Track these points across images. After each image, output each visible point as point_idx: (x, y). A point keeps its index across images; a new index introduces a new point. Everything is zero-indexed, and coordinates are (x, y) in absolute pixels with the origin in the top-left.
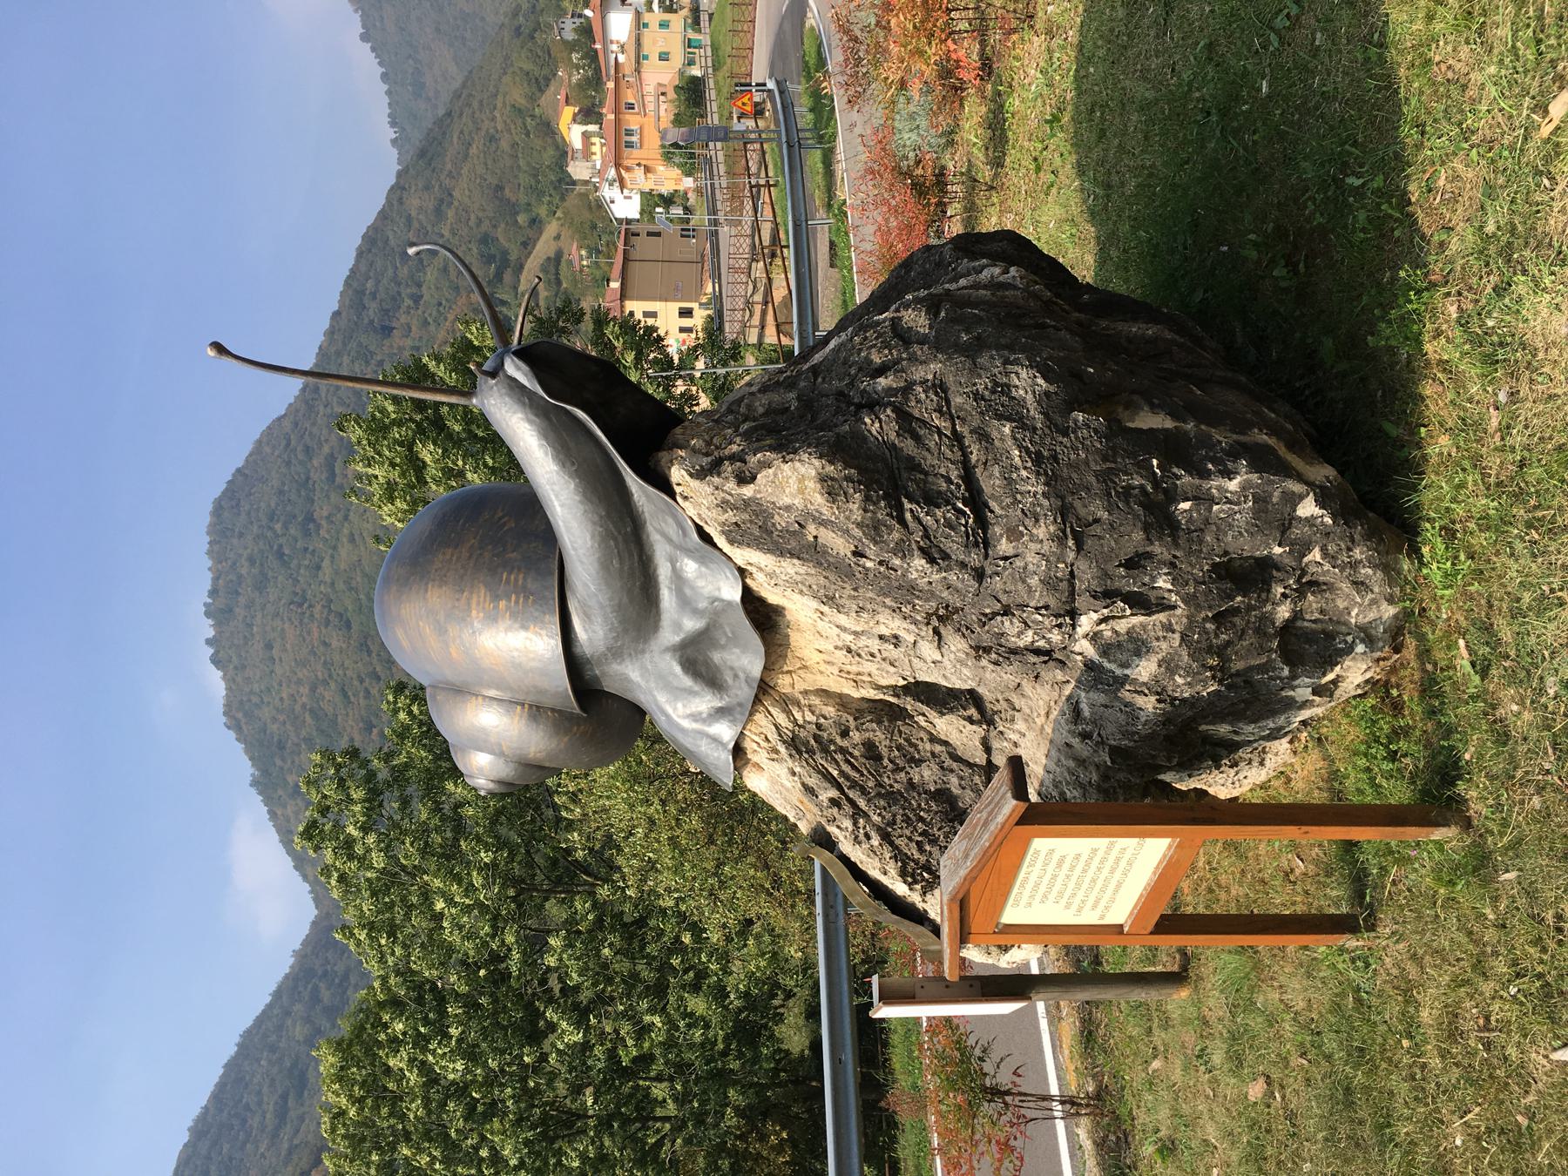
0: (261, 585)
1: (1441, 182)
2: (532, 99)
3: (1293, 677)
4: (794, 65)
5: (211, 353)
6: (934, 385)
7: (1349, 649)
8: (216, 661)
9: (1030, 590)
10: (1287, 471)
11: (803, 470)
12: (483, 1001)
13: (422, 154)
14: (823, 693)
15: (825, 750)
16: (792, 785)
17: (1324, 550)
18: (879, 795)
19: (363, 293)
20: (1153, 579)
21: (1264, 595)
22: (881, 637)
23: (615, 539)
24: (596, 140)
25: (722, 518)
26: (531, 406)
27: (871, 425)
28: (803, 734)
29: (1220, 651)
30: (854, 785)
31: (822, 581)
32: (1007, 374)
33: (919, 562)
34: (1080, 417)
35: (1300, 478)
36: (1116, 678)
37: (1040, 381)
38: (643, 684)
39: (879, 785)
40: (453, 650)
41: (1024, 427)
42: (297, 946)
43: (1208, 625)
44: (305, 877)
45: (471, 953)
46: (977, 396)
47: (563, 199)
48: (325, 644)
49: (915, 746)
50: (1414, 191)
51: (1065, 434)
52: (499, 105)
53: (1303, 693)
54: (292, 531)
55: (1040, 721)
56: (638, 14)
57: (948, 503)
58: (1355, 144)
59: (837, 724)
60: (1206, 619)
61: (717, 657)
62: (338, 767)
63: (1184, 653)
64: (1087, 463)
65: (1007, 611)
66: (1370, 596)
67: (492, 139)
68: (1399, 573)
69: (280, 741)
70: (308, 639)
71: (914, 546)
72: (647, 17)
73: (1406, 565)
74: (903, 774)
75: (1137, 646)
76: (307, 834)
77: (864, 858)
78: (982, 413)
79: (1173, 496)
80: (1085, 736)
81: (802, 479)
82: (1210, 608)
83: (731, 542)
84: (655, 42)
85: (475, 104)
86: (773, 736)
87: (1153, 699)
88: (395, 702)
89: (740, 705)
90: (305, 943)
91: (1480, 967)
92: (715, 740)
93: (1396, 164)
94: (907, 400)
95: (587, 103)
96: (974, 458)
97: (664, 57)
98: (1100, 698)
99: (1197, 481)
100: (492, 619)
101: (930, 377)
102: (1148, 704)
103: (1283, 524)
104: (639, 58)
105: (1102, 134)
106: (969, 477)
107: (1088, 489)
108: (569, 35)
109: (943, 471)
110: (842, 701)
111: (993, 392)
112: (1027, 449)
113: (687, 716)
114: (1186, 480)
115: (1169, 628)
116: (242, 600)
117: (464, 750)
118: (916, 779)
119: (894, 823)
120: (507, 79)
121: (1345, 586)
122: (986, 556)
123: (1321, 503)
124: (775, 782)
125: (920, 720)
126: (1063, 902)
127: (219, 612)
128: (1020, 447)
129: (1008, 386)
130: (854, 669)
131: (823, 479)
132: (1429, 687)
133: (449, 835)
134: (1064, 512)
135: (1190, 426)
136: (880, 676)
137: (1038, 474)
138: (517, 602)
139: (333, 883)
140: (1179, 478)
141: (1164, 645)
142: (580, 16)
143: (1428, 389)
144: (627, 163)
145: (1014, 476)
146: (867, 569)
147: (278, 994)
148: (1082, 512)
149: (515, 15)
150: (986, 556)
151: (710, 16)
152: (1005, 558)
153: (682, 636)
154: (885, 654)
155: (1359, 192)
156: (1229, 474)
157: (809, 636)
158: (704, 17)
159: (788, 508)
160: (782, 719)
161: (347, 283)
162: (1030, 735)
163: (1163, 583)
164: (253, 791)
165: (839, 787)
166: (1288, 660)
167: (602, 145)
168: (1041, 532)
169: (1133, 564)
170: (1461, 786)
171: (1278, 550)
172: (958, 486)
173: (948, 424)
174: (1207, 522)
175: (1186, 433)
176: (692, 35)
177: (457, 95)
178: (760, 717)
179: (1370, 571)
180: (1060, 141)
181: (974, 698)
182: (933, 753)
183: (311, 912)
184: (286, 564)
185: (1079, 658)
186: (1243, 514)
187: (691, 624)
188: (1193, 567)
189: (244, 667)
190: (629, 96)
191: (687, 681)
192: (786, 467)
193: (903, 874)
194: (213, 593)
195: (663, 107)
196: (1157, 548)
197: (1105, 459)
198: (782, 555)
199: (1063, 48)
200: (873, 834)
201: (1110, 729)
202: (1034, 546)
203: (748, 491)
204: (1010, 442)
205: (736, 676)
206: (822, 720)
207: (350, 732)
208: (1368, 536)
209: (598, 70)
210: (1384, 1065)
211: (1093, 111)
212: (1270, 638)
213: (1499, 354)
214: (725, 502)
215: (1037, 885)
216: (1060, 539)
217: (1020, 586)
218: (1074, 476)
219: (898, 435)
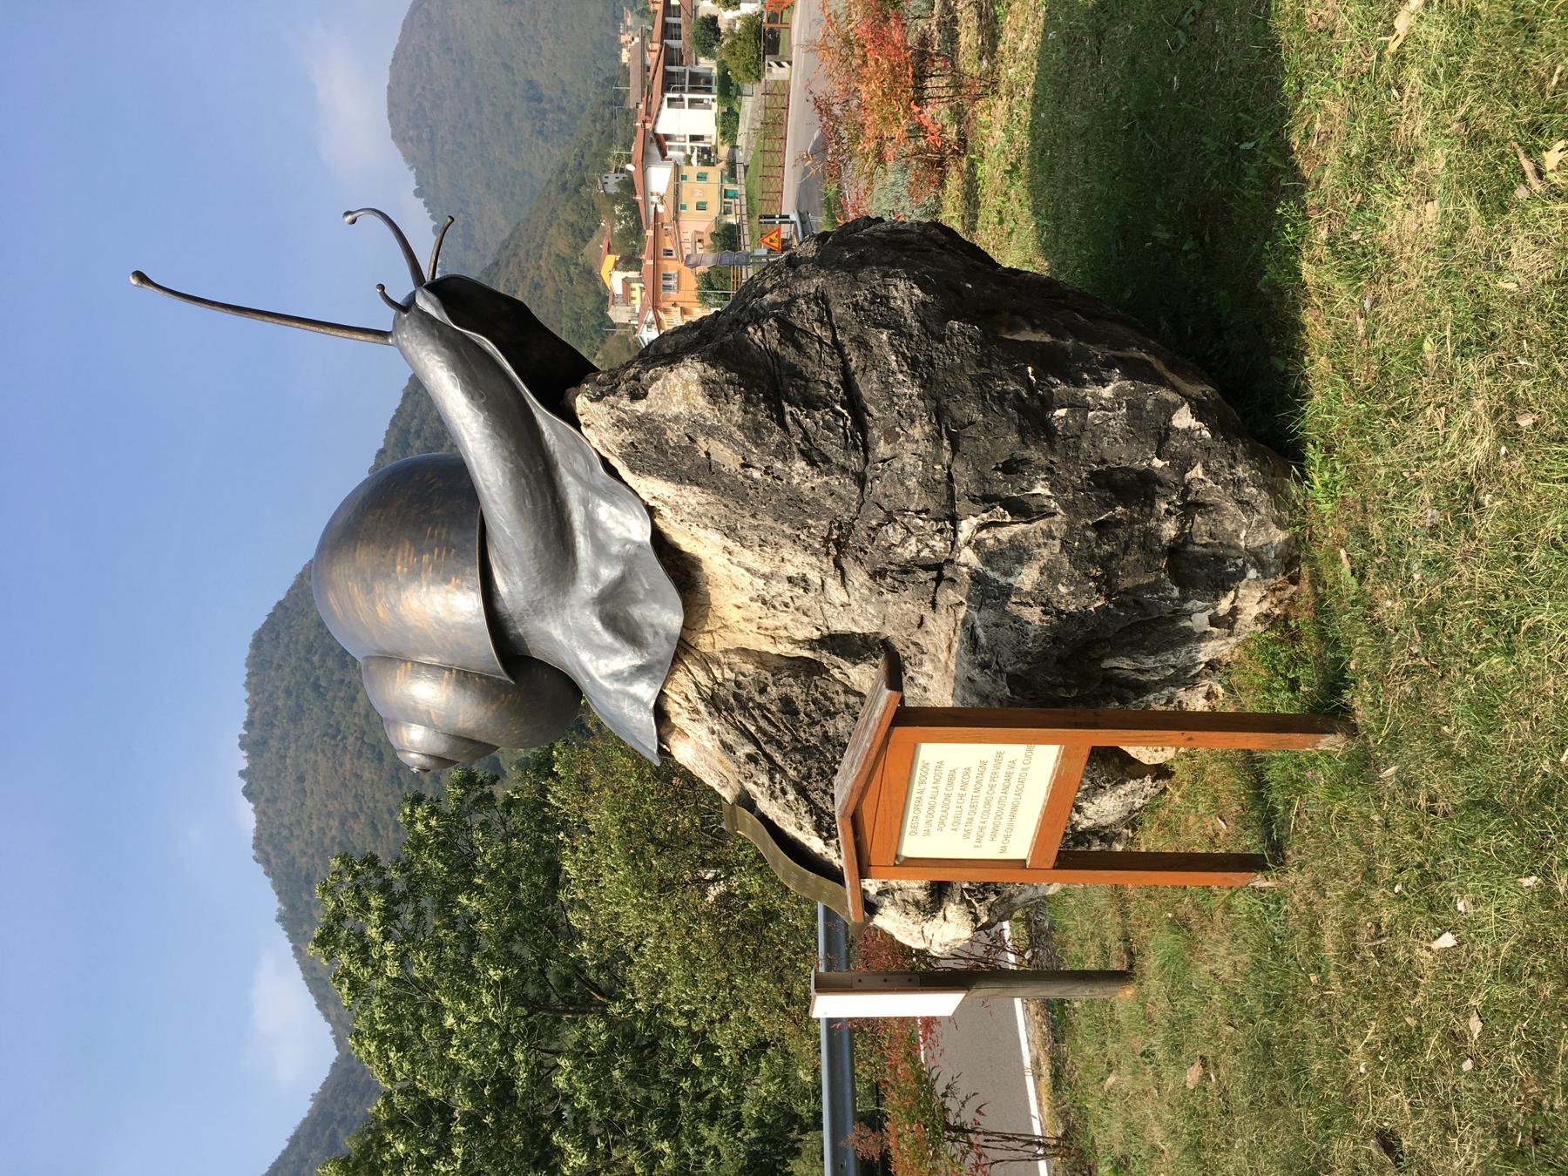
0: (295, 718)
1: (1318, 126)
2: (576, 248)
3: (1185, 599)
4: (818, 200)
5: (134, 281)
6: (816, 298)
7: (1242, 574)
8: (248, 793)
9: (909, 493)
10: (1160, 381)
11: (686, 374)
12: (488, 1120)
14: (744, 652)
15: (744, 707)
16: (711, 744)
17: (1206, 467)
18: (795, 749)
19: (408, 432)
20: (1031, 485)
21: (1147, 510)
22: (790, 579)
23: (526, 477)
24: (636, 286)
25: (619, 439)
26: (440, 338)
27: (754, 335)
28: (722, 692)
29: (1104, 563)
30: (771, 740)
31: (723, 510)
32: (886, 286)
33: (800, 465)
34: (956, 325)
35: (1174, 389)
36: (1000, 587)
37: (917, 291)
38: (565, 642)
39: (795, 739)
40: (380, 610)
41: (901, 334)
42: (317, 1090)
43: (1089, 533)
44: (327, 1017)
45: (478, 1071)
46: (857, 307)
47: (603, 342)
48: (357, 776)
49: (831, 700)
50: (1295, 139)
51: (941, 340)
52: (545, 255)
53: (1200, 621)
54: (329, 663)
55: (943, 657)
56: (677, 167)
57: (826, 406)
58: (1247, 111)
59: (756, 681)
60: (1086, 526)
61: (637, 612)
62: (356, 875)
63: (1065, 560)
64: (962, 368)
65: (890, 518)
66: (1257, 517)
67: (537, 286)
68: (1287, 497)
69: (307, 876)
70: (341, 771)
71: (795, 449)
72: (685, 170)
73: (1294, 490)
74: (818, 728)
75: (1019, 553)
76: (321, 942)
77: (780, 813)
78: (861, 322)
79: (1048, 403)
80: (984, 666)
81: (685, 386)
82: (1090, 515)
83: (632, 469)
84: (692, 192)
85: (522, 254)
86: (693, 695)
87: (1038, 609)
88: (412, 816)
89: (660, 662)
90: (324, 1086)
91: (1369, 874)
92: (636, 700)
93: (1278, 118)
94: (790, 311)
95: (628, 251)
96: (853, 365)
97: (701, 206)
98: (989, 615)
99: (1072, 389)
100: (415, 574)
101: (813, 290)
102: (1033, 615)
103: (1162, 436)
104: (678, 207)
105: (1051, 169)
107: (963, 393)
108: (612, 189)
109: (823, 377)
110: (761, 659)
111: (873, 303)
112: (904, 356)
113: (602, 667)
114: (1061, 388)
115: (1049, 535)
116: (277, 732)
117: (395, 722)
119: (810, 776)
120: (553, 231)
121: (1230, 506)
122: (866, 461)
123: (1198, 413)
124: (698, 748)
125: (835, 672)
126: (961, 828)
127: (254, 745)
128: (896, 353)
129: (887, 298)
130: (769, 623)
131: (704, 382)
132: (1322, 610)
133: (463, 951)
134: (939, 414)
135: (1069, 342)
136: (792, 632)
137: (914, 376)
138: (439, 555)
139: (345, 990)
140: (1054, 386)
141: (1045, 552)
142: (622, 171)
143: (1307, 317)
144: (664, 305)
145: (891, 380)
146: (755, 481)
147: (295, 1140)
148: (957, 414)
149: (562, 172)
150: (866, 461)
151: (746, 168)
152: (884, 461)
153: (600, 587)
154: (798, 603)
155: (1251, 155)
156: (1103, 382)
157: (726, 590)
158: (740, 169)
159: (676, 419)
160: (701, 677)
161: (393, 423)
162: (937, 676)
163: (1041, 489)
164: (279, 927)
165: (756, 743)
166: (1178, 582)
167: (642, 289)
168: (916, 432)
169: (1012, 467)
170: (1347, 694)
171: (1158, 463)
172: (837, 390)
173: (829, 334)
174: (1083, 428)
175: (1064, 349)
176: (728, 186)
178: (680, 676)
179: (1254, 491)
180: (1019, 189)
181: (886, 645)
182: (847, 706)
183: (332, 1053)
184: (321, 696)
185: (965, 570)
186: (1118, 420)
187: (609, 573)
188: (1071, 473)
189: (276, 799)
191: (607, 638)
192: (672, 376)
193: (818, 828)
194: (249, 725)
196: (1034, 454)
197: (980, 364)
198: (681, 482)
199: (1020, 103)
200: (789, 789)
201: (1006, 654)
202: (910, 447)
203: (640, 407)
204: (887, 348)
205: (656, 633)
206: (741, 678)
207: (363, 842)
208: (1250, 454)
209: (638, 221)
210: (1296, 1007)
211: (1044, 151)
212: (1157, 556)
213: (1361, 263)
214: (620, 420)
215: (932, 808)
216: (936, 439)
217: (899, 489)
218: (949, 379)
219: (780, 343)
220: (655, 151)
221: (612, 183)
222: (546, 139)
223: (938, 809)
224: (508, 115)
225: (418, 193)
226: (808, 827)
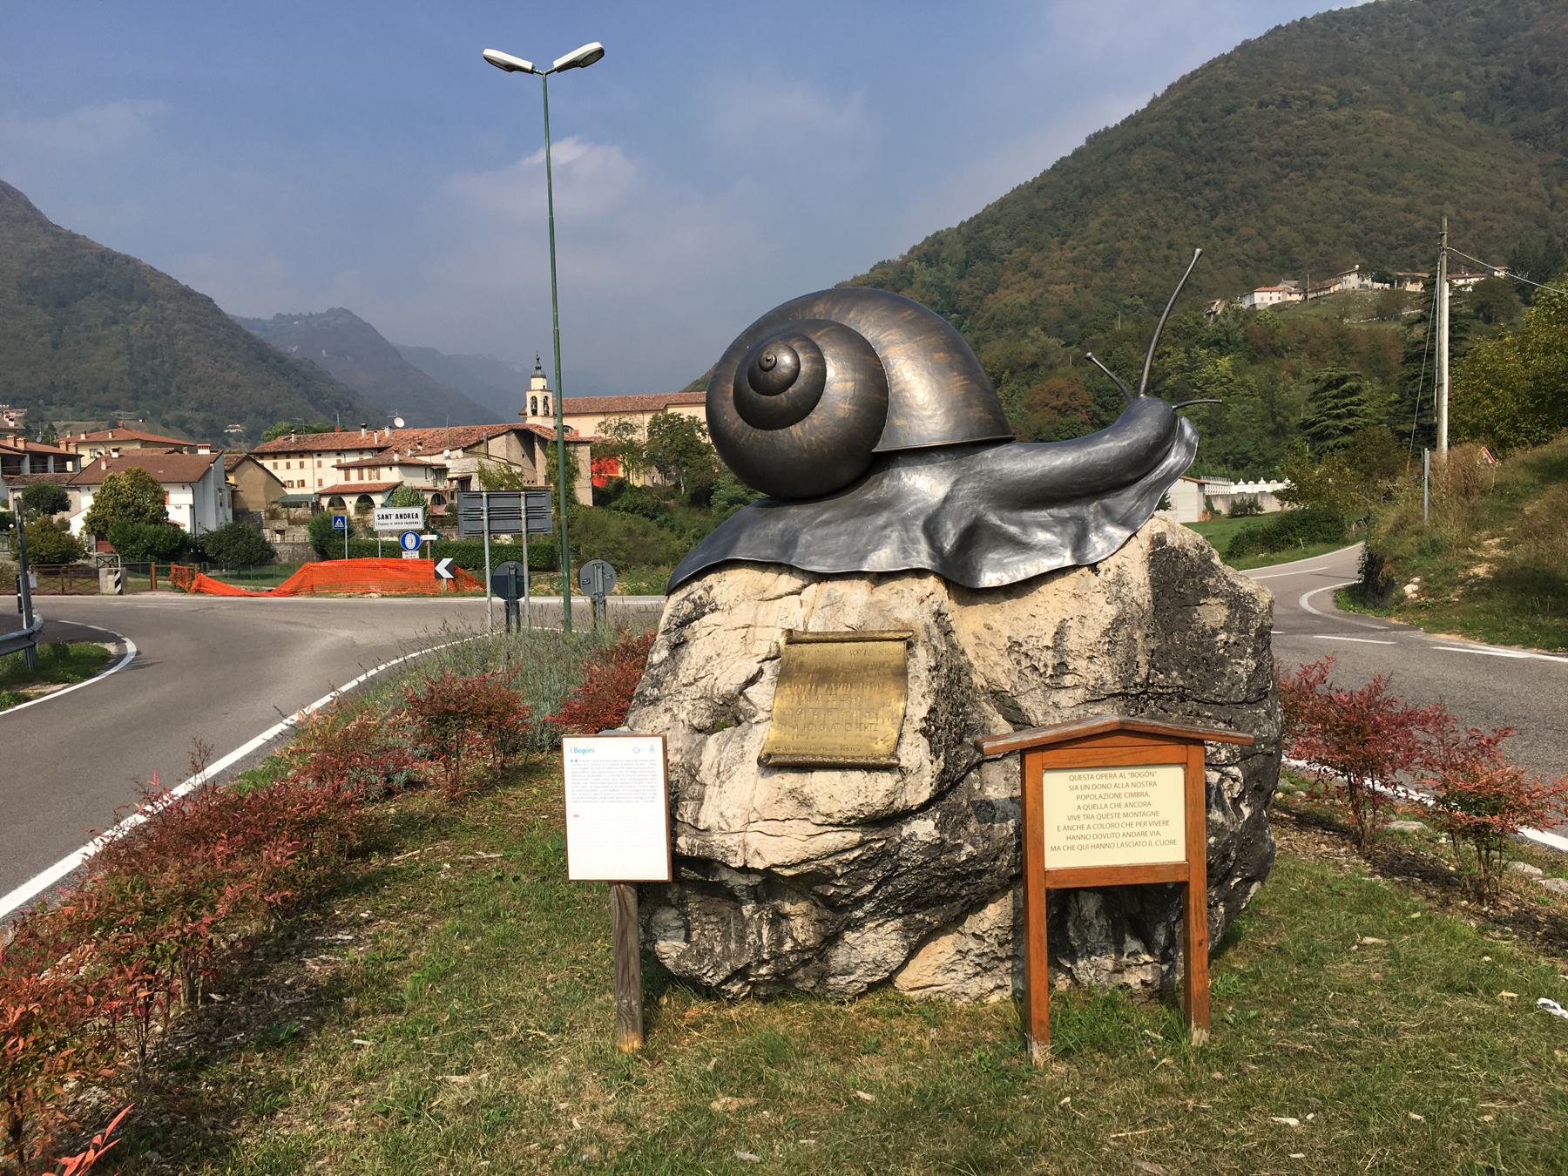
223: (1104, 791)
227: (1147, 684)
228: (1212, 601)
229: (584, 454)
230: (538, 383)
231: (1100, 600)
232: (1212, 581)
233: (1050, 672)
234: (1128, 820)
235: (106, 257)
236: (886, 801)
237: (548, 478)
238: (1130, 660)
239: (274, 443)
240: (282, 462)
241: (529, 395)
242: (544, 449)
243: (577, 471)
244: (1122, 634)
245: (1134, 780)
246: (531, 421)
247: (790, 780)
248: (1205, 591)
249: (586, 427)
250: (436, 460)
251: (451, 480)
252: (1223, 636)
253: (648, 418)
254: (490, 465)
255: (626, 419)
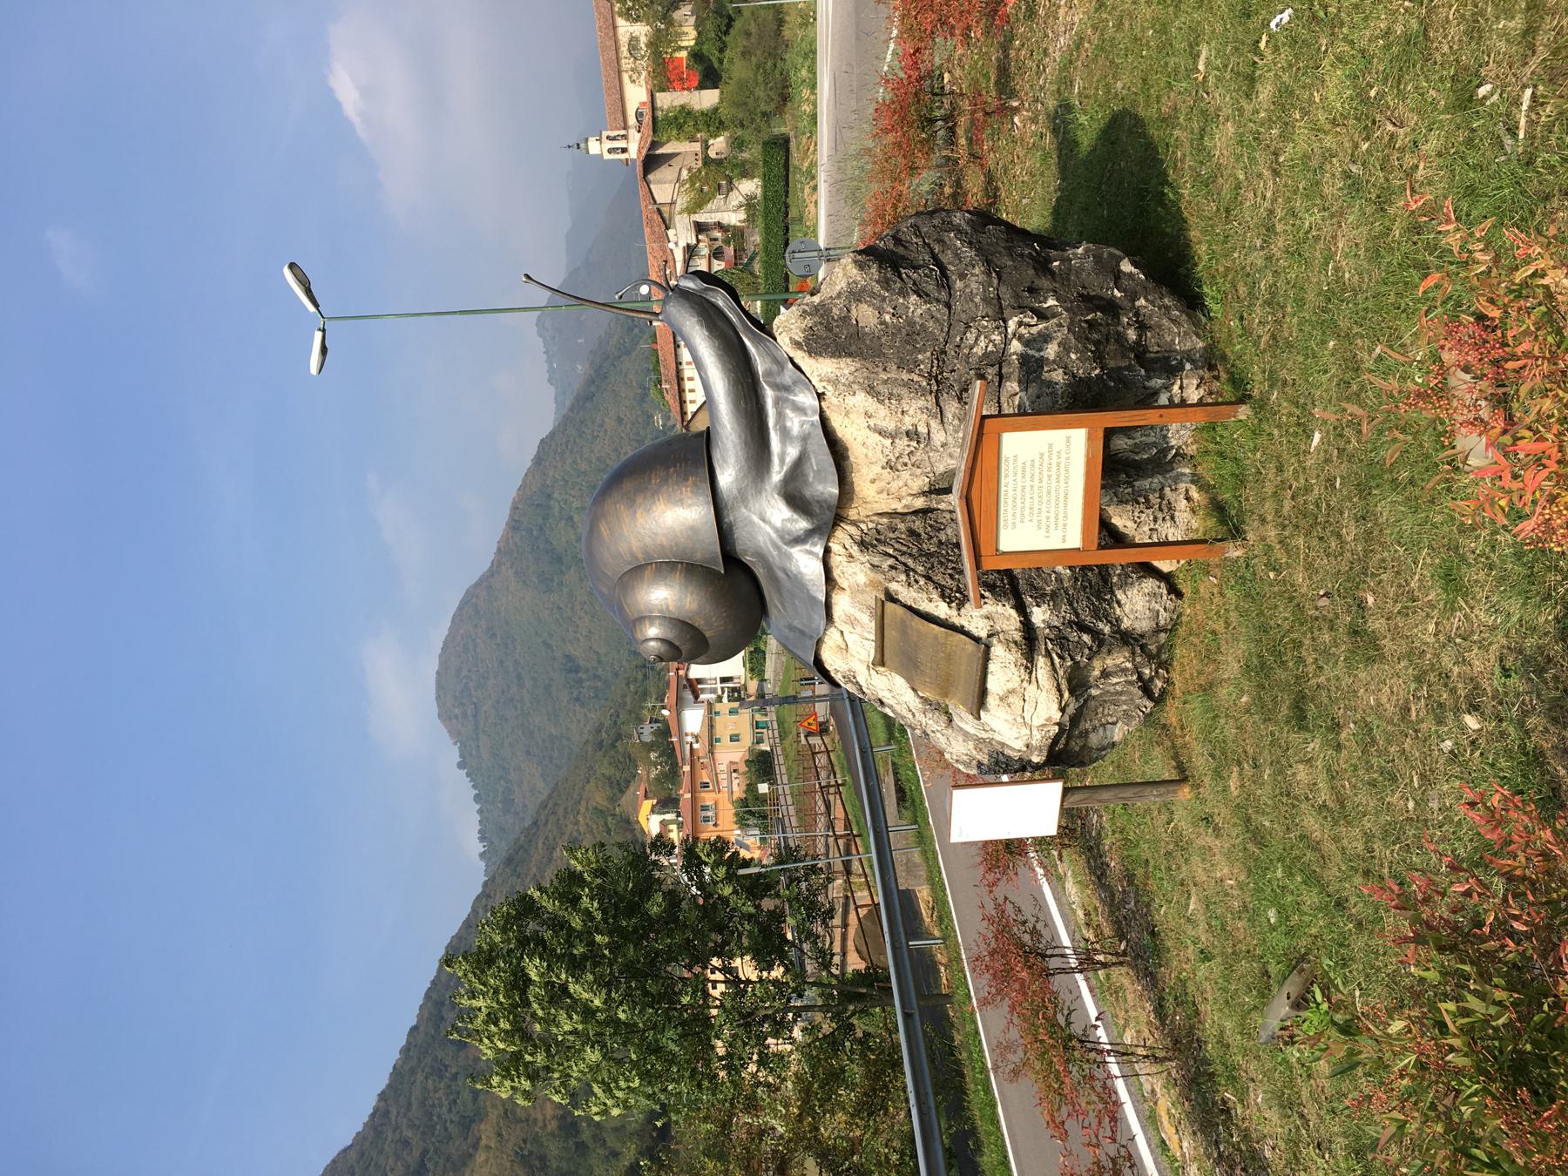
2: (613, 800)
13: (509, 861)
19: (443, 1004)
30: (904, 553)
33: (914, 298)
52: (582, 810)
72: (718, 707)
75: (1045, 338)
84: (726, 727)
85: (560, 812)
95: (664, 794)
97: (735, 738)
103: (1118, 276)
104: (713, 741)
106: (935, 257)
108: (647, 737)
110: (893, 514)
114: (1053, 253)
118: (944, 539)
131: (855, 262)
134: (988, 262)
161: (428, 996)
163: (1051, 302)
168: (977, 271)
177: (543, 806)
178: (839, 533)
186: (1089, 263)
190: (705, 777)
195: (735, 782)
203: (816, 299)
216: (989, 274)
220: (688, 695)
221: (648, 732)
222: (583, 705)
223: (1019, 501)
224: (547, 688)
225: (461, 766)
226: (935, 596)
227: (930, 376)
228: (854, 312)
229: (666, 100)
230: (594, 147)
231: (851, 400)
232: (836, 311)
233: (914, 444)
234: (1045, 479)
235: (514, 525)
236: (1014, 649)
237: (692, 139)
238: (908, 385)
239: (671, 402)
240: (689, 396)
241: (607, 156)
242: (662, 145)
243: (683, 107)
244: (881, 388)
245: (1011, 474)
246: (633, 153)
247: (992, 701)
248: (845, 319)
249: (636, 95)
250: (679, 256)
251: (698, 241)
252: (887, 318)
253: (620, 22)
254: (682, 202)
255: (624, 50)
